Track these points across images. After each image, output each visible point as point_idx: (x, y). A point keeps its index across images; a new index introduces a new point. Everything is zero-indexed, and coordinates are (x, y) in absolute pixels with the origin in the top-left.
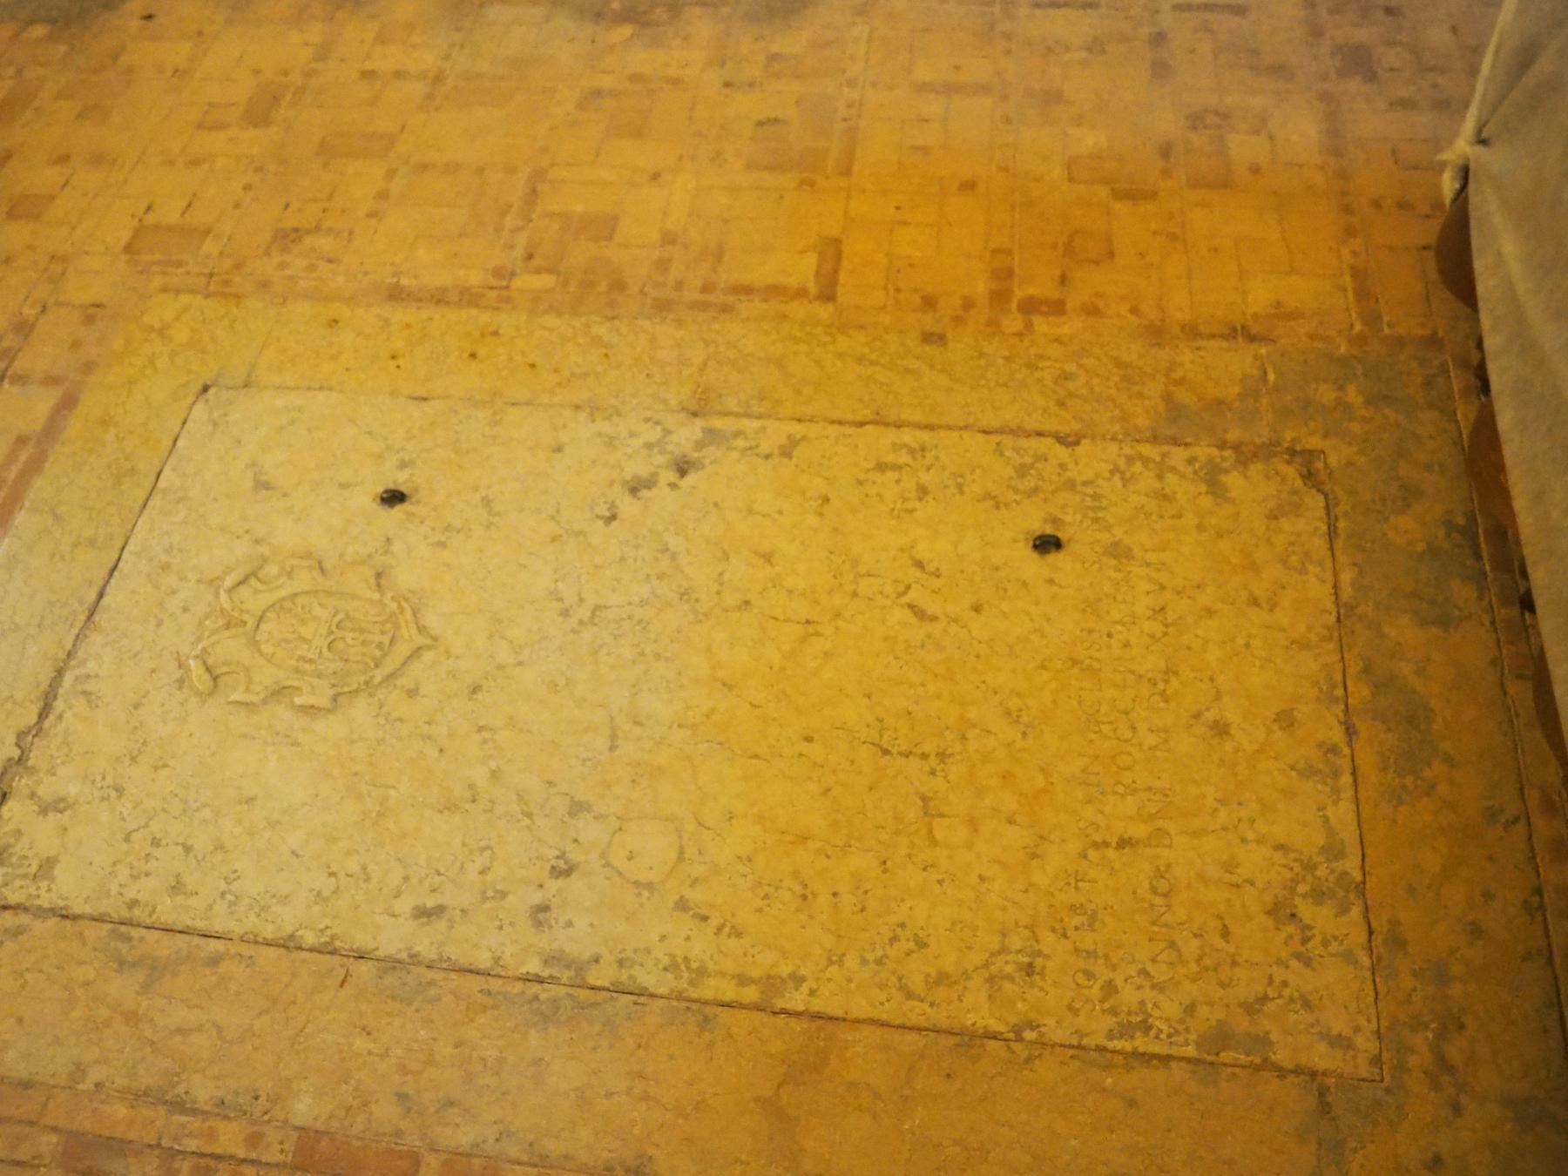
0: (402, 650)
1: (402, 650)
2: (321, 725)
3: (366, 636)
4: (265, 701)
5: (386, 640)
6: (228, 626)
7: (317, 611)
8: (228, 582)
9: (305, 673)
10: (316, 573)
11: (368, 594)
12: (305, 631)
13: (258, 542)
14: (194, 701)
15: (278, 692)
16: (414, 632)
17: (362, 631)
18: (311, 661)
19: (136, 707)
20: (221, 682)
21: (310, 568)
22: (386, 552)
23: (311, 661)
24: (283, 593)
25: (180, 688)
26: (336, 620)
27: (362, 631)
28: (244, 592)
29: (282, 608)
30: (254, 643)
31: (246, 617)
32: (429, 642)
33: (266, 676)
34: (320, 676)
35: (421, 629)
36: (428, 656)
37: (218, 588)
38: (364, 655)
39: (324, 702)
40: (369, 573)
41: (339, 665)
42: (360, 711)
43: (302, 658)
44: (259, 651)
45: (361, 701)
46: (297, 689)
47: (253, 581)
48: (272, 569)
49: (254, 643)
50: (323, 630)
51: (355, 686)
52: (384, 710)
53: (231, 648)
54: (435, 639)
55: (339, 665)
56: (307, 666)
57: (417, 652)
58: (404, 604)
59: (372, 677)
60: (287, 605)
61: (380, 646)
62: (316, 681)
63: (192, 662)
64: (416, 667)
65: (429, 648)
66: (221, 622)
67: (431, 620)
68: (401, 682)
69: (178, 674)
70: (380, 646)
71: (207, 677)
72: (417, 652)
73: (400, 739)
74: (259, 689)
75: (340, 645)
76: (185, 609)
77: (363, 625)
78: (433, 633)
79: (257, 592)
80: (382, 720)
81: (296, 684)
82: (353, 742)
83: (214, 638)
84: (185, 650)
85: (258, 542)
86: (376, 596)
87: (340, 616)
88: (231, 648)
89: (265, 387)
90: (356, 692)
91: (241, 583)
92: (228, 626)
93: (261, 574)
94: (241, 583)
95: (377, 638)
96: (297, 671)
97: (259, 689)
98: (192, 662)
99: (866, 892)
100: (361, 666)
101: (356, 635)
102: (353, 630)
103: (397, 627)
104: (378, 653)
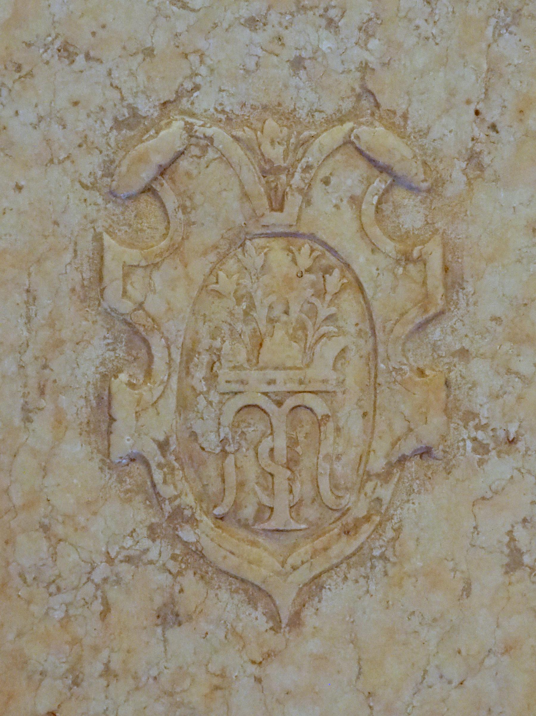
0: (261, 560)
1: (261, 560)
2: (75, 449)
3: (282, 476)
4: (110, 314)
5: (281, 518)
6: (268, 170)
7: (329, 350)
8: (376, 136)
9: (187, 370)
10: (415, 316)
11: (381, 447)
12: (280, 347)
13: (473, 158)
14: (89, 164)
15: (134, 335)
16: (304, 575)
17: (292, 463)
18: (212, 377)
19: (67, 52)
20: (146, 203)
21: (426, 299)
22: (481, 448)
23: (212, 377)
24: (362, 261)
25: (118, 124)
26: (310, 400)
27: (292, 463)
28: (351, 177)
29: (328, 270)
30: (238, 240)
31: (294, 202)
32: (285, 615)
33: (167, 296)
34: (183, 406)
35: (315, 586)
36: (256, 620)
37: (353, 115)
38: (241, 485)
39: (124, 443)
40: (430, 431)
41: (211, 441)
42: (122, 519)
43: (217, 356)
44: (222, 259)
45: (139, 514)
46: (148, 373)
47: (379, 184)
48: (411, 214)
49: (238, 240)
50: (284, 382)
51: (167, 491)
52: (123, 568)
53: (220, 193)
54: (296, 621)
55: (211, 441)
56: (200, 374)
57: (255, 593)
58: (367, 529)
59: (193, 521)
60: (334, 281)
61: (264, 511)
62: (172, 401)
63: (178, 125)
64: (226, 603)
65: (274, 616)
66: (275, 153)
67: (336, 597)
68: (189, 580)
69: (146, 107)
70: (264, 511)
71: (146, 174)
72: (255, 593)
73: (66, 621)
74: (136, 292)
75: (255, 427)
76: (297, 64)
77: (307, 462)
78: (308, 614)
79: (355, 201)
80: (102, 570)
81: (159, 365)
82: (45, 528)
83: (237, 153)
84: (205, 101)
85: (473, 158)
86: (378, 464)
87: (320, 406)
88: (220, 193)
89: (407, 110)
90: (155, 498)
91: (372, 161)
92: (268, 170)
93: (399, 194)
94: (372, 161)
95: (282, 503)
96: (189, 354)
97: (136, 292)
98: (178, 125)
99: (158, 617)
100: (215, 487)
101: (282, 453)
102: (293, 443)
103: (315, 530)
104: (248, 512)
